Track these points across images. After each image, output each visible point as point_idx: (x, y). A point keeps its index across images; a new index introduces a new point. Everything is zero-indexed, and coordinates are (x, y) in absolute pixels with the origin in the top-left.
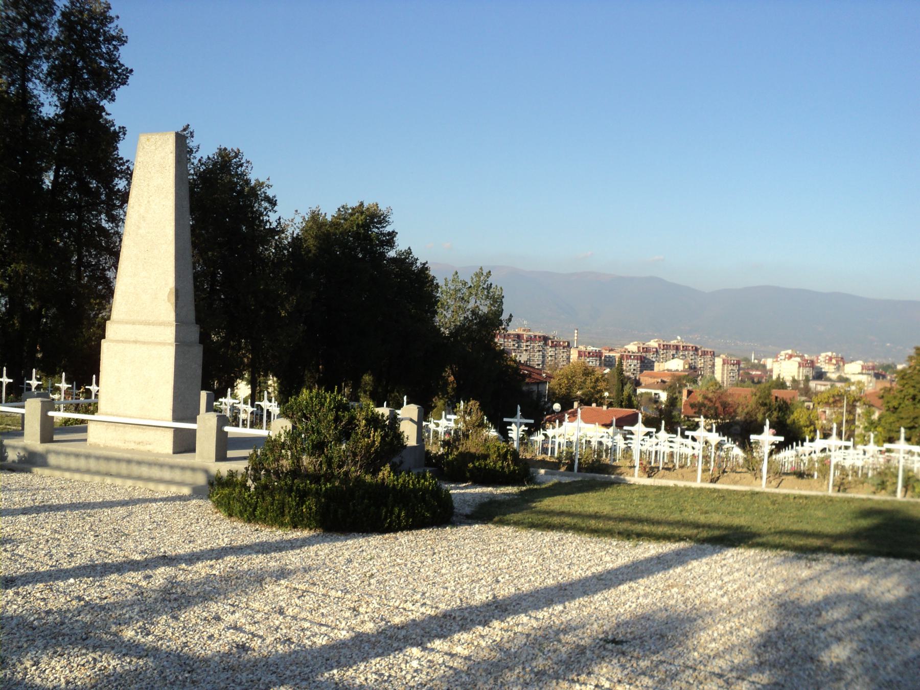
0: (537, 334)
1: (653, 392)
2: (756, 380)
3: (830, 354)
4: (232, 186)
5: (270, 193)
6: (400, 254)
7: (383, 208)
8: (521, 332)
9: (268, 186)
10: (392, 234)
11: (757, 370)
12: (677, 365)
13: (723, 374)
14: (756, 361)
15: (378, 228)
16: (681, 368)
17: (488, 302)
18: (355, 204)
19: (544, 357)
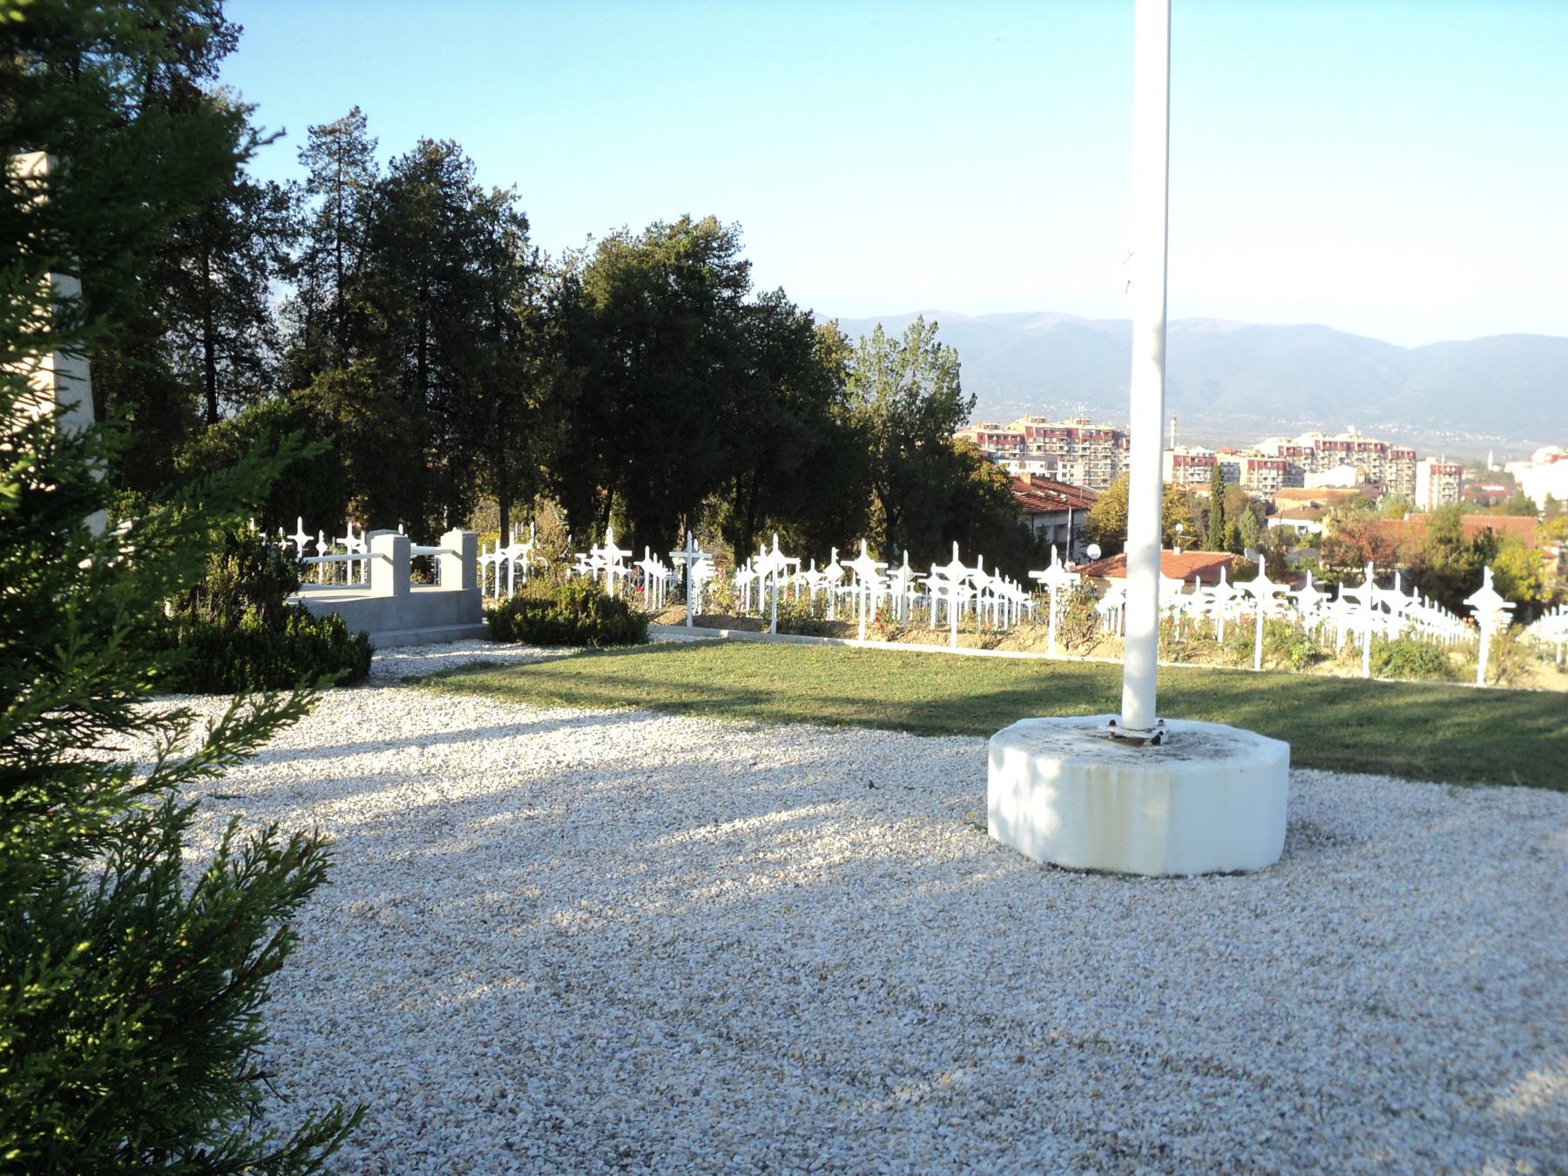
0: (1102, 427)
2: (1492, 501)
4: (441, 203)
5: (518, 208)
7: (726, 223)
9: (513, 197)
10: (743, 267)
11: (1497, 483)
12: (1344, 477)
14: (1496, 469)
15: (719, 257)
16: (1351, 482)
17: (934, 374)
18: (674, 220)
19: (1114, 466)
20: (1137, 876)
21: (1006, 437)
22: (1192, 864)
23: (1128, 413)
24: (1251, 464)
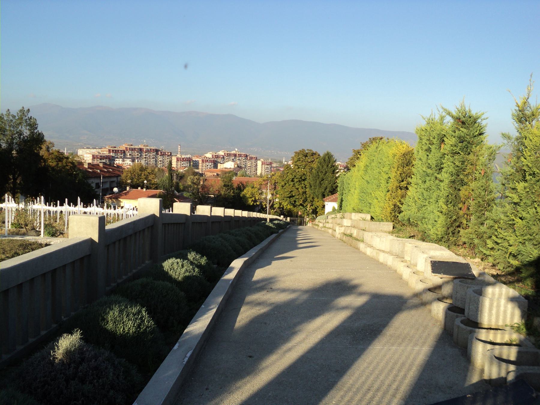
0: (152, 148)
8: (142, 147)
12: (230, 165)
13: (262, 170)
14: (286, 163)
19: (156, 161)
20: (410, 237)
21: (118, 151)
24: (203, 161)
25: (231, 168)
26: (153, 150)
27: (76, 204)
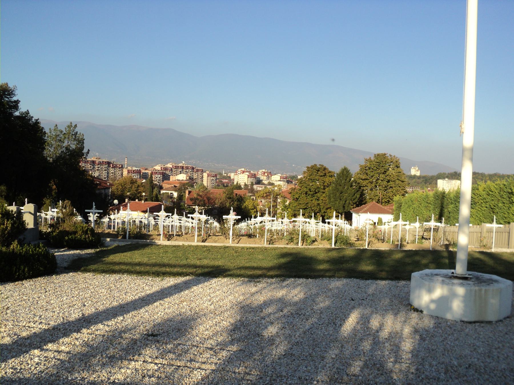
0: (104, 160)
1: (170, 192)
3: (264, 170)
6: (22, 114)
7: (11, 86)
8: (95, 160)
10: (17, 102)
11: (226, 179)
12: (182, 177)
13: (208, 182)
16: (185, 179)
19: (108, 173)
22: (501, 318)
23: (473, 176)
25: (183, 180)
26: (105, 162)
27: (441, 222)
